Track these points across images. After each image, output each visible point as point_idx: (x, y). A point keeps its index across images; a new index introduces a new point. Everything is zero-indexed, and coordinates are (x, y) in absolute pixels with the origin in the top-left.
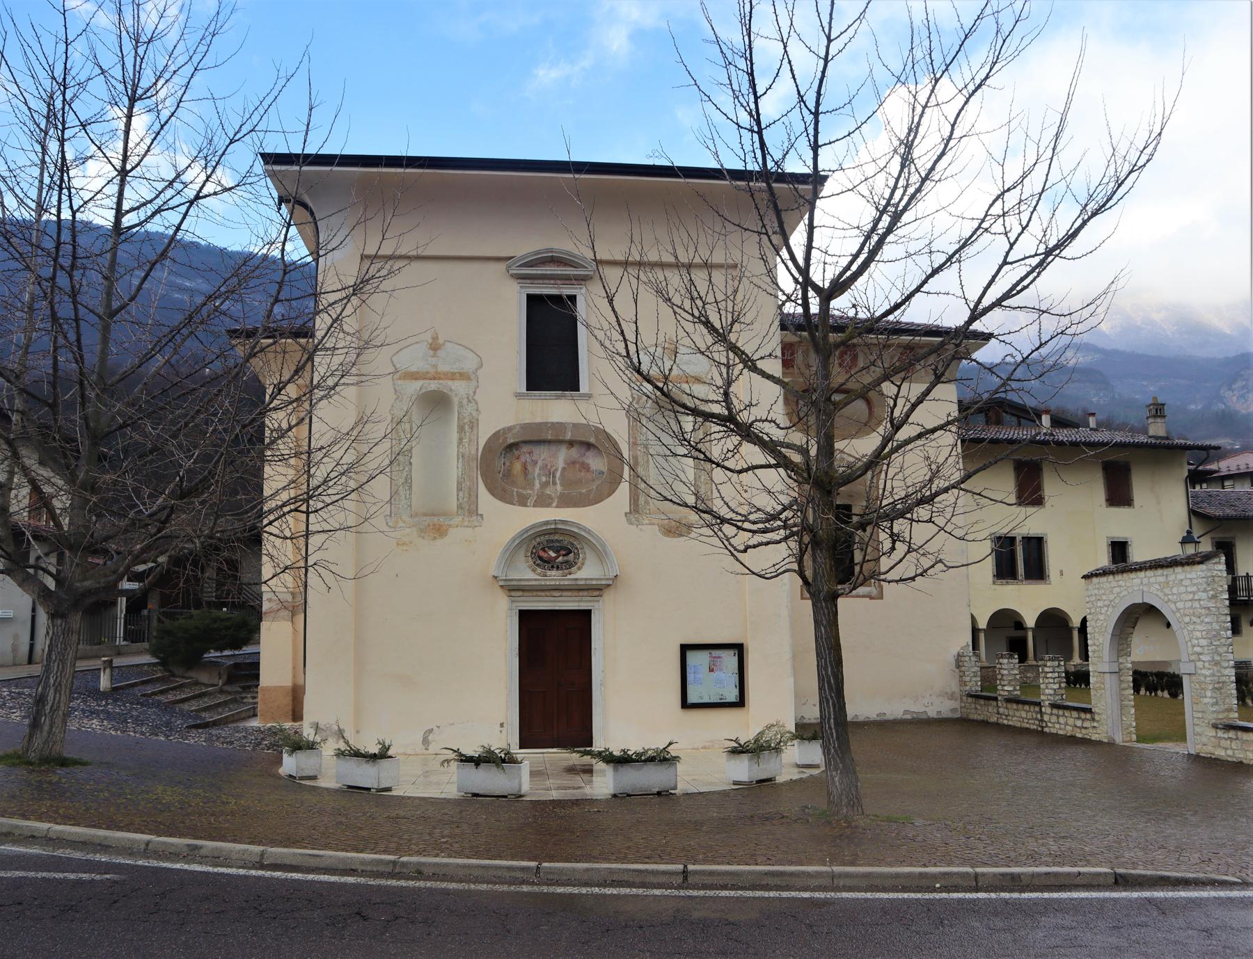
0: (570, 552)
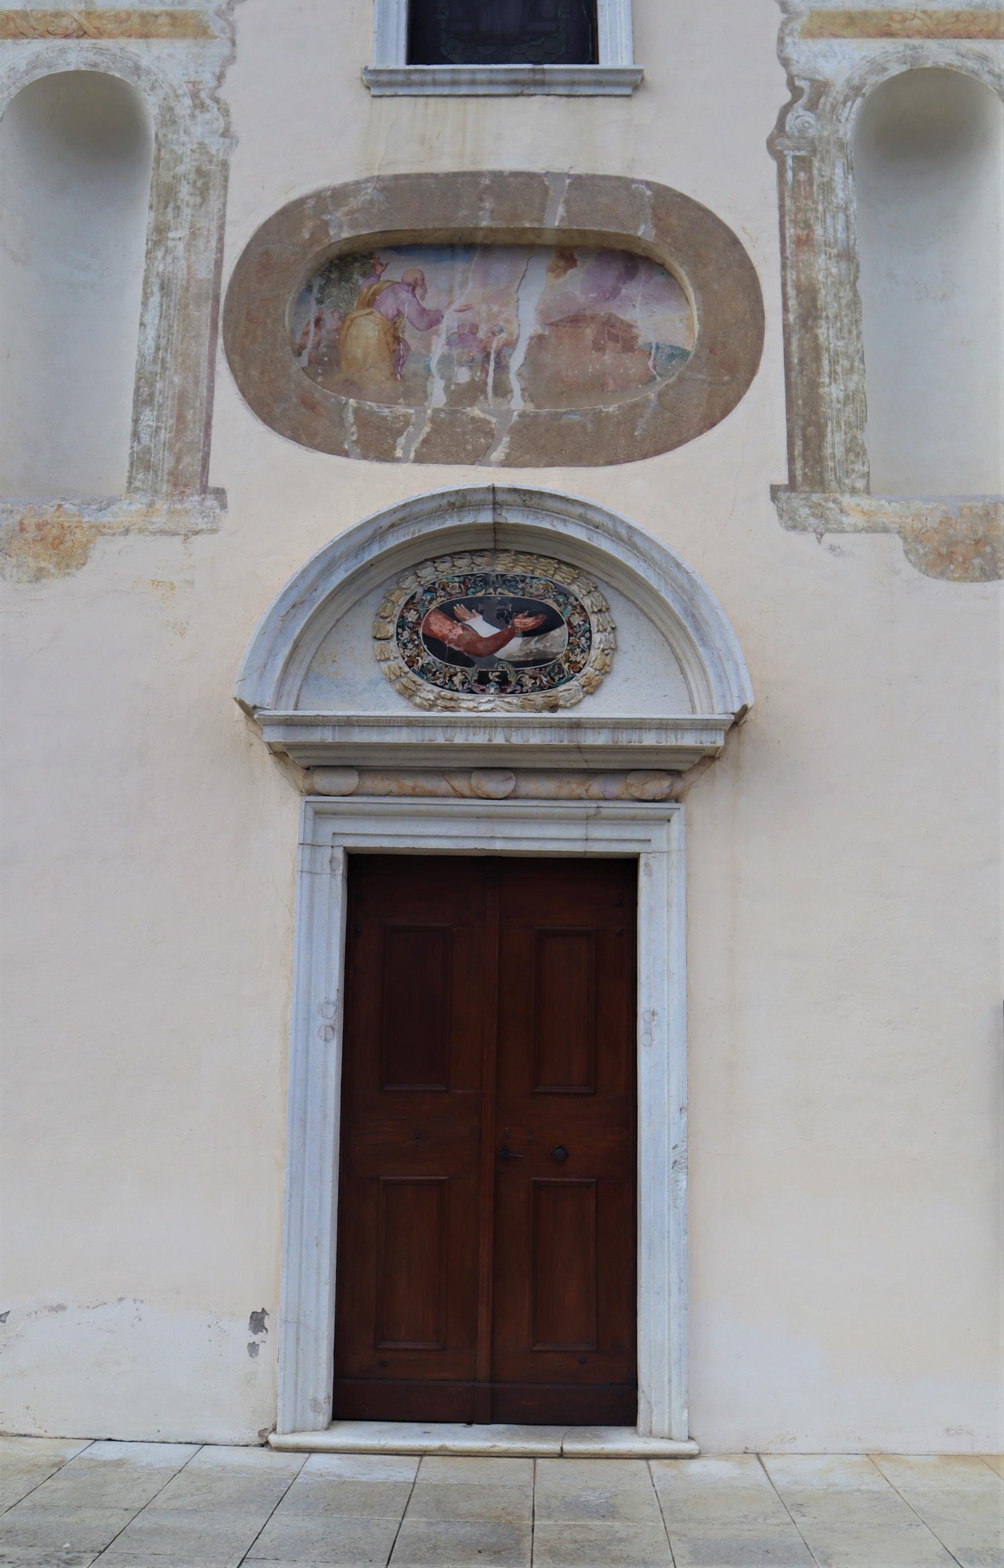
0: (551, 622)
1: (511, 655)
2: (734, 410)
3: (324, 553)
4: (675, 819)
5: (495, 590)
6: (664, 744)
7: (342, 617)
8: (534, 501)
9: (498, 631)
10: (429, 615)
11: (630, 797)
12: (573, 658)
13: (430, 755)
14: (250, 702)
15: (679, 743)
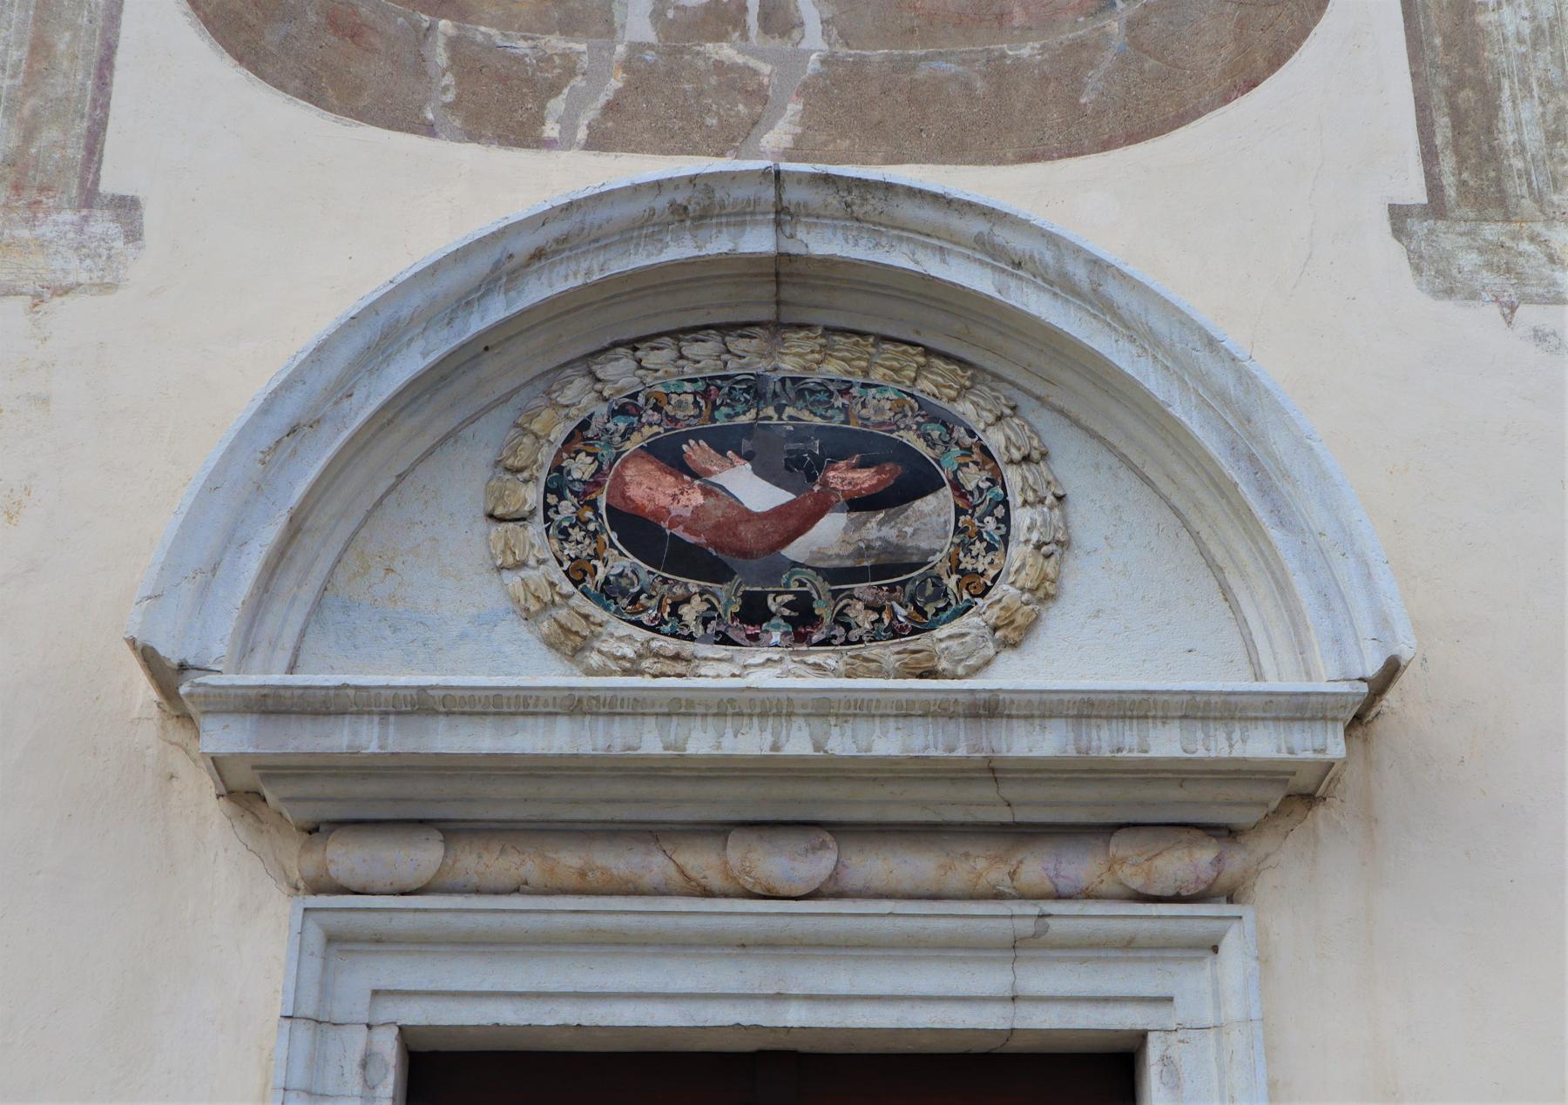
0: (915, 480)
1: (822, 555)
2: (1296, 56)
3: (372, 309)
4: (1231, 944)
5: (780, 410)
6: (1201, 753)
7: (413, 467)
8: (875, 203)
9: (790, 497)
10: (623, 465)
11: (1116, 889)
12: (967, 563)
13: (622, 789)
14: (171, 652)
15: (1238, 752)
